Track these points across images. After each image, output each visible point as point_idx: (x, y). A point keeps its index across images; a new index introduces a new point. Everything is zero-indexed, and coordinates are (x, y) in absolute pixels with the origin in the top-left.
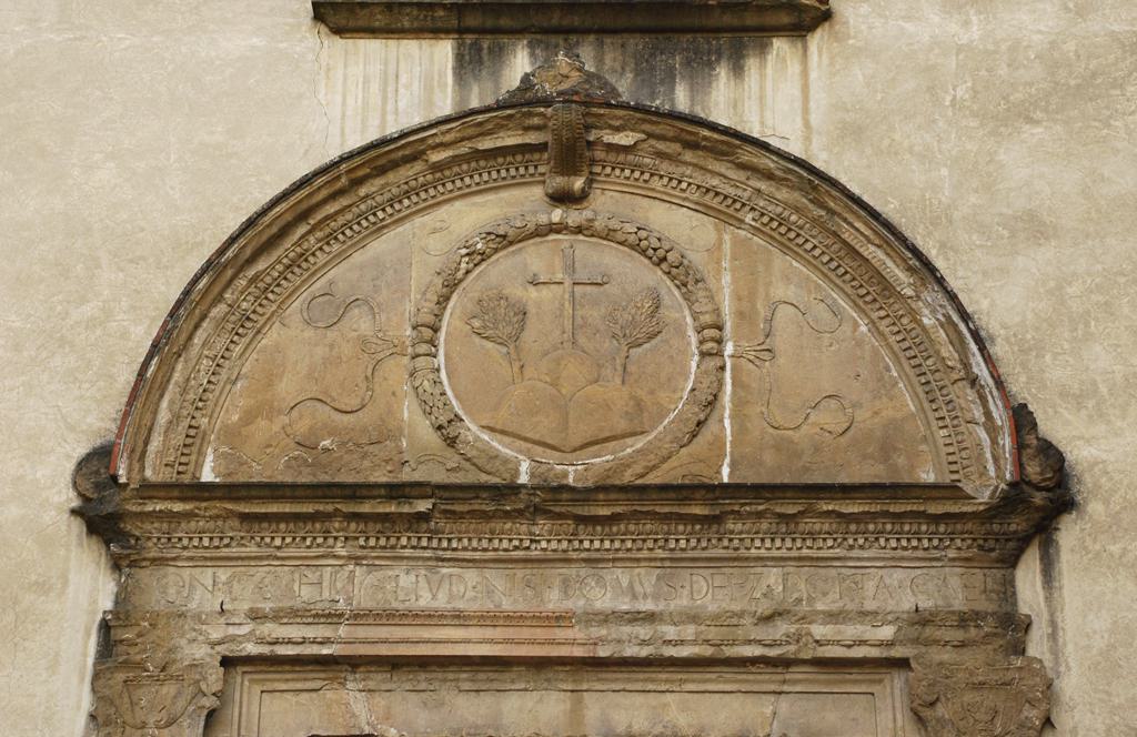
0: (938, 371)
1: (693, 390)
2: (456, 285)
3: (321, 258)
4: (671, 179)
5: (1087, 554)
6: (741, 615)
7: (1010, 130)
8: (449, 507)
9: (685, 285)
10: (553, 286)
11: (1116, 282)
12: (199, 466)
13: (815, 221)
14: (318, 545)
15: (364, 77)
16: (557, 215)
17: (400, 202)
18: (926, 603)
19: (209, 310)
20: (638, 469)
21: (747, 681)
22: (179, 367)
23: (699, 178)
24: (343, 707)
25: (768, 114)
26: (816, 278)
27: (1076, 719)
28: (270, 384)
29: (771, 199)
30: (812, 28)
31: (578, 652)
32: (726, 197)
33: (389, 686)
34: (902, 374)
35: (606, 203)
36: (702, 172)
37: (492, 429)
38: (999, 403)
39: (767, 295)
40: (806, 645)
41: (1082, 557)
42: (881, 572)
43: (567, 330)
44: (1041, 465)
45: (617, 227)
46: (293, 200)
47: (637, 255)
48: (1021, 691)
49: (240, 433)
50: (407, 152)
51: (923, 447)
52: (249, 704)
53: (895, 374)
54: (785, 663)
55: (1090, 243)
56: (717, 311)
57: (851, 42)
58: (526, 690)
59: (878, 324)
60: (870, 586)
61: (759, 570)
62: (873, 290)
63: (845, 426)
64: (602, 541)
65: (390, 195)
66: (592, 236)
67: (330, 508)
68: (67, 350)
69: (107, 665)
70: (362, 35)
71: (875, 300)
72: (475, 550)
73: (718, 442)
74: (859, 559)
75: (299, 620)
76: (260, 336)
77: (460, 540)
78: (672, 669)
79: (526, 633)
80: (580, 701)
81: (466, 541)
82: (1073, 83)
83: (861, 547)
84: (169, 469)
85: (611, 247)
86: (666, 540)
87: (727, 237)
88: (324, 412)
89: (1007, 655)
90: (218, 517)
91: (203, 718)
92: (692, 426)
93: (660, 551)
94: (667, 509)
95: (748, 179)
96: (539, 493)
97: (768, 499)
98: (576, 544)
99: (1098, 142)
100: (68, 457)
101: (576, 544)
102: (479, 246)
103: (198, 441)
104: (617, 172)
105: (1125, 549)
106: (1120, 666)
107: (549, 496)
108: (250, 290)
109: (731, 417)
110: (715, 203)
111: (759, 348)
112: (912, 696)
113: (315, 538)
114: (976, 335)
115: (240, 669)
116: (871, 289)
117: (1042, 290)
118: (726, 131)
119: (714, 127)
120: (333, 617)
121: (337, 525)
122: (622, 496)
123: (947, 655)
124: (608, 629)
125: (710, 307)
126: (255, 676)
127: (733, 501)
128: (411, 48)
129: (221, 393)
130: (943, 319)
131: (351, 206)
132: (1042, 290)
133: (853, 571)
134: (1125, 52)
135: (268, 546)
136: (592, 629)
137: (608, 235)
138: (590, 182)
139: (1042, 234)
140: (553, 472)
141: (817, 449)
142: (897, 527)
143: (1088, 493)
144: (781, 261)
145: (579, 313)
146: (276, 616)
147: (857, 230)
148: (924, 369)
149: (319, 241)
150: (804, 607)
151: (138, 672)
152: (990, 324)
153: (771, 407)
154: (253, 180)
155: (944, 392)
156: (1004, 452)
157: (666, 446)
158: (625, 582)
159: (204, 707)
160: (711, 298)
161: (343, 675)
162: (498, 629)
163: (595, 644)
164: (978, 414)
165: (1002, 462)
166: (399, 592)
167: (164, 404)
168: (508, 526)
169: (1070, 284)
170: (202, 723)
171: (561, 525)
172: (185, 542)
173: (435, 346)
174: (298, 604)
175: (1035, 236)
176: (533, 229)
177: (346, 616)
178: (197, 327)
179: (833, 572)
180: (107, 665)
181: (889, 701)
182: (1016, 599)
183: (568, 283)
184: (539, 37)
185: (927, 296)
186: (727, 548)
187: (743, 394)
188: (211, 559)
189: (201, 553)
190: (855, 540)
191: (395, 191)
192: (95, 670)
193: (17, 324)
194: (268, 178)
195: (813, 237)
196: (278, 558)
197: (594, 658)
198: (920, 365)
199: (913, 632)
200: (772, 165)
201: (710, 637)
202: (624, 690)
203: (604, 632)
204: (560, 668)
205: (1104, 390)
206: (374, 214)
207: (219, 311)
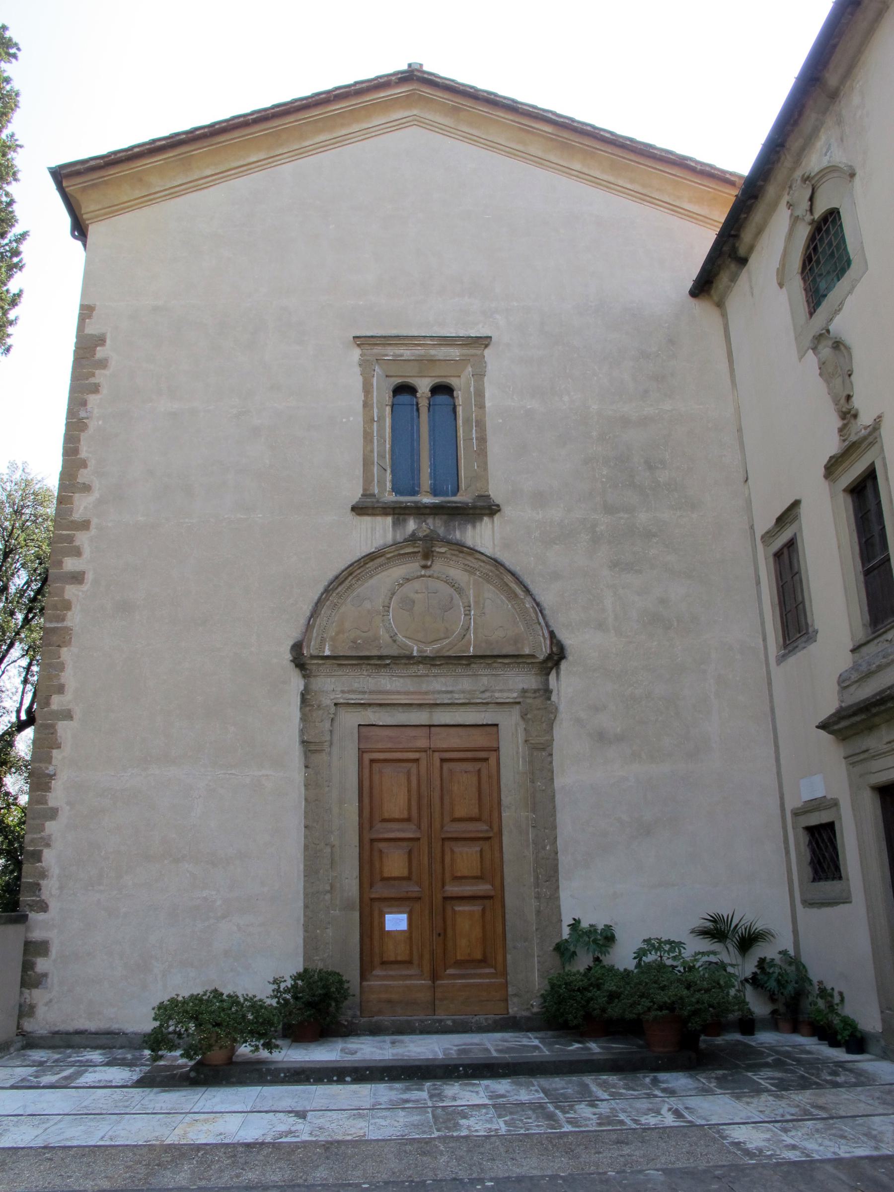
3: (356, 586)
13: (497, 575)
16: (423, 572)
18: (526, 687)
31: (432, 702)
35: (438, 566)
54: (487, 703)
56: (469, 602)
79: (413, 697)
112: (521, 712)
118: (471, 549)
120: (364, 693)
128: (379, 519)
137: (438, 578)
146: (349, 692)
164: (541, 633)
207: (328, 603)
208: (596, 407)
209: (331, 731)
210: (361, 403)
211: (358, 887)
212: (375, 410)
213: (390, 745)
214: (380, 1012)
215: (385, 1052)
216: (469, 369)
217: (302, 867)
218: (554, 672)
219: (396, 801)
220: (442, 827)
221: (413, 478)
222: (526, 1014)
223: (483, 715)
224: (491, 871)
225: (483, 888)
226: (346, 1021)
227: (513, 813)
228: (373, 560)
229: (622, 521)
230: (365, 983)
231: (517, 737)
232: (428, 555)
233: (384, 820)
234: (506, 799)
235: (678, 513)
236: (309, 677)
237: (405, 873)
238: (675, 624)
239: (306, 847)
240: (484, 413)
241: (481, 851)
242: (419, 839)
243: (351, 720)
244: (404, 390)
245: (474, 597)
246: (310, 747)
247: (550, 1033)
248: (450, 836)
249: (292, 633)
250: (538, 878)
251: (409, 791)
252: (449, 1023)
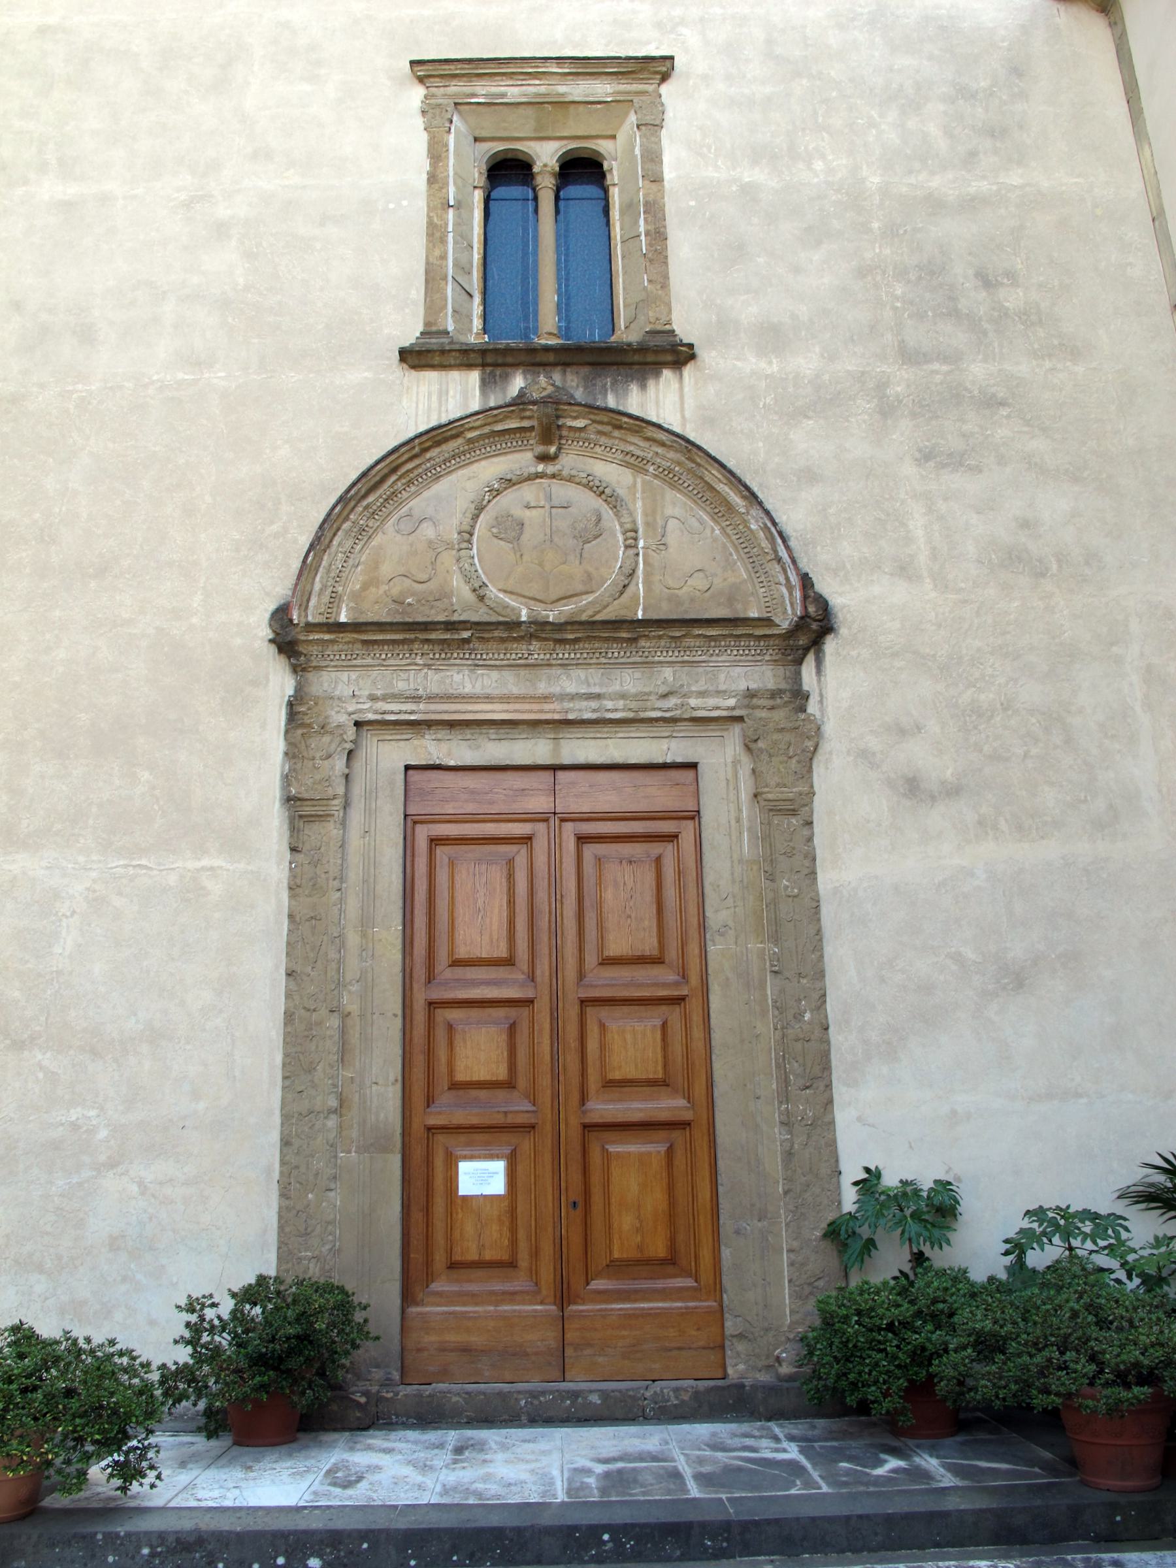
13: (689, 471)
30: (685, 363)
31: (557, 717)
35: (570, 461)
54: (674, 720)
56: (634, 522)
79: (517, 706)
118: (637, 418)
120: (416, 699)
128: (455, 375)
146: (384, 698)
164: (782, 579)
207: (346, 525)
208: (876, 180)
209: (347, 776)
210: (425, 176)
211: (399, 1103)
212: (452, 189)
213: (470, 808)
214: (444, 1374)
215: (429, 1481)
216: (633, 118)
217: (279, 1058)
218: (810, 659)
219: (480, 917)
220: (581, 975)
221: (526, 318)
222: (764, 1377)
223: (664, 745)
224: (687, 1071)
225: (668, 1105)
226: (366, 1394)
227: (731, 948)
228: (438, 444)
229: (938, 378)
230: (413, 1310)
231: (737, 788)
233: (456, 963)
234: (717, 916)
235: (1048, 364)
237: (502, 1073)
238: (1055, 567)
239: (289, 1017)
240: (661, 191)
241: (664, 1026)
242: (530, 1002)
243: (389, 756)
244: (508, 170)
245: (645, 514)
246: (302, 810)
247: (821, 1423)
248: (597, 993)
249: (270, 586)
250: (787, 1082)
251: (511, 903)
252: (595, 1399)
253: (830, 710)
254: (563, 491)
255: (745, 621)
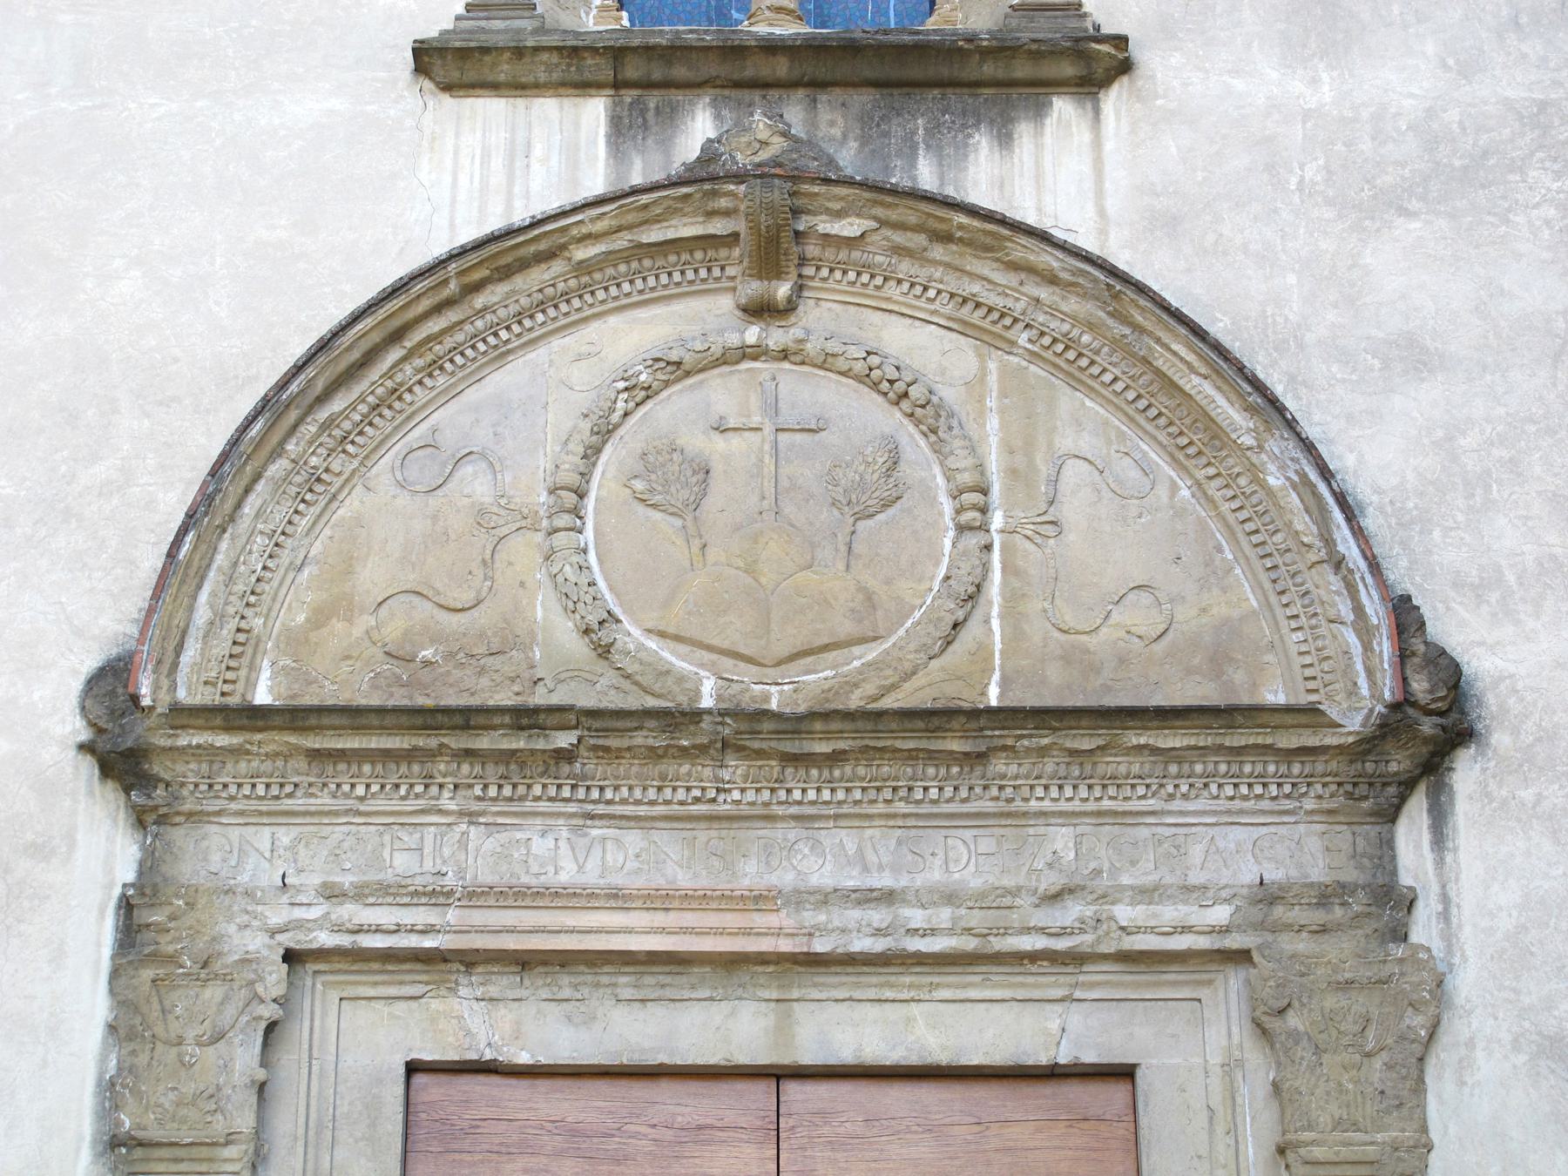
0: (1289, 550)
1: (947, 578)
2: (609, 432)
4: (912, 285)
5: (1490, 802)
6: (1015, 892)
7: (1378, 224)
8: (601, 742)
9: (934, 431)
10: (747, 434)
11: (1523, 431)
12: (251, 684)
13: (1117, 344)
14: (417, 796)
15: (483, 147)
16: (752, 334)
17: (531, 317)
18: (1274, 874)
19: (264, 467)
20: (870, 689)
21: (1023, 985)
22: (224, 546)
23: (953, 283)
24: (454, 1021)
25: (1048, 199)
26: (1117, 423)
27: (1474, 1026)
28: (348, 572)
29: (1053, 311)
30: (1106, 82)
31: (785, 946)
32: (990, 310)
33: (518, 993)
34: (1239, 555)
35: (824, 317)
36: (958, 274)
37: (662, 635)
38: (1373, 593)
39: (1050, 445)
40: (1108, 934)
41: (1483, 807)
42: (1211, 831)
43: (767, 494)
44: (1430, 680)
45: (838, 349)
46: (381, 314)
47: (867, 390)
48: (1403, 991)
49: (307, 640)
50: (543, 246)
51: (1269, 658)
52: (324, 1015)
53: (1230, 557)
54: (1076, 959)
55: (1488, 377)
56: (980, 468)
57: (1159, 102)
58: (711, 999)
59: (1206, 487)
60: (1197, 852)
61: (1042, 830)
62: (1195, 439)
63: (1162, 628)
64: (819, 790)
65: (518, 308)
66: (803, 363)
67: (433, 743)
68: (74, 524)
69: (130, 958)
70: (480, 92)
71: (1200, 453)
72: (638, 802)
73: (982, 654)
74: (1182, 813)
75: (390, 899)
76: (335, 504)
77: (616, 788)
78: (918, 969)
79: (689, 919)
80: (788, 1015)
81: (628, 786)
82: (1457, 163)
83: (1185, 797)
84: (209, 689)
85: (830, 379)
86: (910, 789)
87: (992, 366)
88: (424, 609)
89: (1383, 942)
90: (277, 754)
91: (261, 1033)
92: (946, 628)
93: (902, 804)
94: (911, 745)
95: (1021, 284)
96: (729, 721)
97: (1055, 729)
98: (782, 794)
99: (1494, 243)
100: (75, 672)
101: (782, 794)
102: (643, 378)
103: (249, 650)
104: (838, 275)
105: (1540, 794)
106: (1532, 954)
107: (744, 726)
108: (321, 439)
109: (1002, 617)
110: (976, 317)
111: (1039, 520)
112: (1254, 1001)
113: (412, 786)
114: (1341, 499)
115: (311, 967)
116: (1195, 438)
117: (1426, 441)
119: (973, 211)
120: (438, 896)
121: (442, 767)
122: (848, 726)
123: (1303, 945)
124: (829, 913)
125: (969, 462)
126: (331, 978)
127: (1006, 732)
128: (547, 108)
129: (281, 584)
130: (1296, 478)
131: (462, 322)
132: (1426, 441)
133: (1173, 830)
134: (1524, 125)
135: (347, 796)
136: (805, 914)
137: (825, 362)
138: (799, 288)
139: (1425, 365)
140: (747, 695)
141: (1122, 661)
142: (1235, 768)
143: (1493, 718)
144: (1069, 401)
145: (785, 470)
146: (360, 894)
147: (1175, 353)
148: (1268, 549)
149: (419, 371)
150: (1105, 881)
151: (170, 969)
152: (1361, 490)
153: (1058, 602)
154: (327, 290)
155: (1299, 580)
156: (1382, 662)
157: (911, 657)
158: (851, 848)
159: (261, 1018)
160: (973, 450)
161: (453, 978)
162: (672, 914)
163: (810, 935)
164: (1345, 609)
165: (1378, 675)
166: (531, 860)
167: (203, 597)
168: (685, 769)
169: (1464, 433)
170: (260, 1040)
171: (760, 767)
172: (233, 789)
173: (581, 518)
174: (388, 876)
175: (1416, 369)
176: (718, 355)
177: (458, 895)
178: (247, 491)
179: (1144, 832)
180: (130, 958)
181: (1222, 1008)
182: (1395, 867)
183: (768, 429)
184: (726, 92)
185: (1273, 445)
186: (997, 799)
187: (1018, 585)
188: (269, 814)
189: (253, 805)
190: (1176, 786)
191: (524, 301)
192: (114, 965)
193: (8, 491)
194: (348, 288)
195: (1115, 365)
196: (359, 813)
197: (808, 954)
198: (1264, 543)
199: (1256, 913)
200: (1055, 264)
201: (972, 925)
202: (851, 999)
203: (822, 918)
204: (760, 969)
205: (1511, 578)
206: (496, 334)
207: (277, 468)
209: (262, 1087)
223: (1052, 1019)
228: (505, 273)
231: (1233, 1130)
232: (776, 249)
236: (162, 820)
243: (366, 1037)
253: (1468, 936)
254: (805, 392)
255: (1254, 714)
